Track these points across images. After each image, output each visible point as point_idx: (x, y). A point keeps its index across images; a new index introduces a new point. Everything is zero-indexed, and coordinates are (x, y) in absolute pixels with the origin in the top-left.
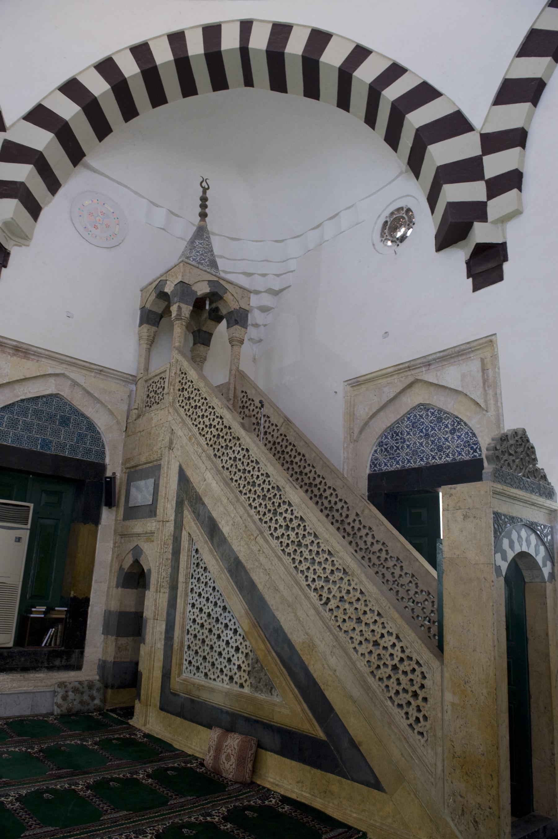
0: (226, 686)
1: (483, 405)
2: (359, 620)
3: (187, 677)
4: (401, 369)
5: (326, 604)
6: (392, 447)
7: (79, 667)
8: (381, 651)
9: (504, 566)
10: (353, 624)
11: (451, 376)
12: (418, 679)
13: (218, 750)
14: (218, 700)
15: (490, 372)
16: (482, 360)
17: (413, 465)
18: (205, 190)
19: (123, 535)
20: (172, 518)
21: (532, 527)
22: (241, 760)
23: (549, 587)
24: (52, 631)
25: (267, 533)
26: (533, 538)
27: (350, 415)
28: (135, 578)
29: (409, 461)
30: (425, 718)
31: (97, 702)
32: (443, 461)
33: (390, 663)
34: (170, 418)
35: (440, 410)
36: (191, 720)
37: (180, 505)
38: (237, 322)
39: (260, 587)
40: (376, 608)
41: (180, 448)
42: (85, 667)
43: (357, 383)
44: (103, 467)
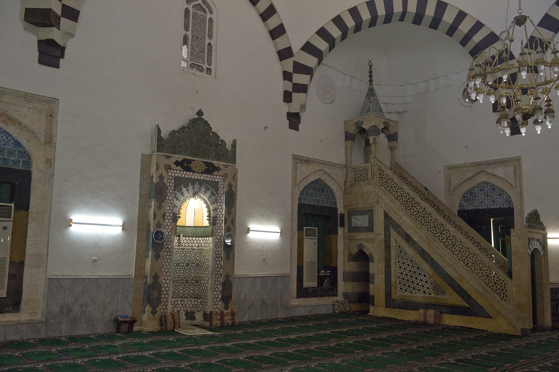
0: (422, 295)
1: (514, 184)
2: (481, 270)
3: (398, 294)
4: (474, 165)
5: (467, 265)
6: (470, 199)
7: (336, 295)
8: (489, 278)
9: (530, 253)
10: (479, 271)
11: (500, 171)
12: (503, 285)
13: (425, 315)
14: (421, 300)
15: (518, 172)
16: (514, 166)
17: (480, 208)
18: (371, 67)
19: (350, 239)
20: (383, 233)
21: (538, 240)
22: (436, 317)
23: (543, 258)
24: (326, 281)
25: (438, 241)
26: (538, 243)
27: (449, 182)
28: (362, 257)
29: (478, 206)
30: (506, 296)
31: (348, 308)
32: (495, 207)
33: (493, 281)
34: (376, 190)
35: (494, 185)
36: (406, 309)
37: (387, 229)
38: (394, 140)
39: (436, 260)
40: (487, 266)
41: (383, 203)
42: (339, 295)
43: (451, 168)
44: (336, 209)
